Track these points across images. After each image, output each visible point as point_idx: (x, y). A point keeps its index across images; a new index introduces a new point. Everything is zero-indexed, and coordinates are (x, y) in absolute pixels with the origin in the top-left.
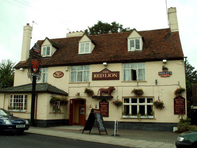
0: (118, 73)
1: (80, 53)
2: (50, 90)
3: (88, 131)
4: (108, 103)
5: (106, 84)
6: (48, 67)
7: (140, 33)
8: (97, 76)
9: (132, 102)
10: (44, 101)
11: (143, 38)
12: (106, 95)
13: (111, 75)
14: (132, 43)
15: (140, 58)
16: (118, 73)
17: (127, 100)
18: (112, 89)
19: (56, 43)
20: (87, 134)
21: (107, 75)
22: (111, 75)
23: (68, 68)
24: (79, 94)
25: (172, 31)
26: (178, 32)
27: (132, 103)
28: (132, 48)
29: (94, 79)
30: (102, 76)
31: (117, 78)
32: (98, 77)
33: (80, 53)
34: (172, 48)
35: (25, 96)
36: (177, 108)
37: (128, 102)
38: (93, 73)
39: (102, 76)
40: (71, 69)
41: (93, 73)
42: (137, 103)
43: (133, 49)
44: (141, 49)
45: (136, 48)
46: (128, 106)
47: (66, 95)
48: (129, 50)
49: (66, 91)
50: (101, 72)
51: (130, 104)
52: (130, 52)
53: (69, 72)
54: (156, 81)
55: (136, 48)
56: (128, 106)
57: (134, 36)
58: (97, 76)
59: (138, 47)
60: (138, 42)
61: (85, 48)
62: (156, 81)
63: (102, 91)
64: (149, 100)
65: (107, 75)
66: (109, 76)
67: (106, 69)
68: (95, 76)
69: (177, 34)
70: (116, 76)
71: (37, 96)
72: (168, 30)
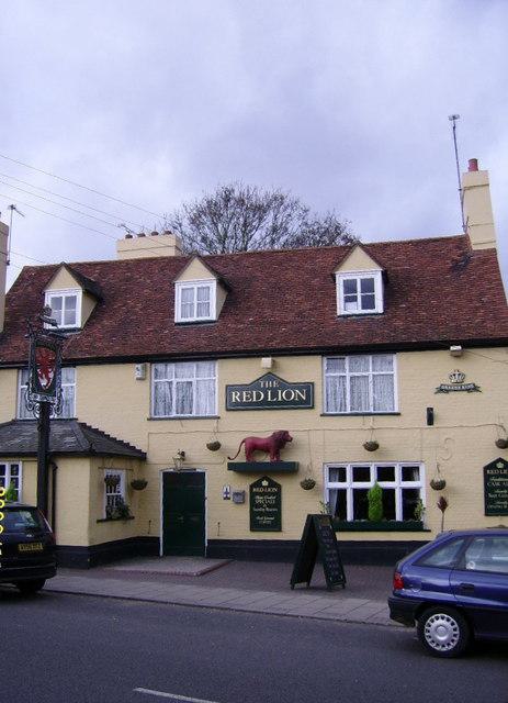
0: (308, 388)
1: (178, 318)
2: (100, 448)
3: (304, 585)
4: (279, 487)
5: (264, 424)
6: (215, 359)
7: (376, 251)
8: (241, 397)
9: (356, 479)
10: (76, 483)
11: (384, 274)
12: (266, 459)
13: (288, 395)
14: (350, 287)
15: (377, 341)
16: (308, 388)
17: (340, 474)
18: (282, 440)
19: (96, 280)
20: (302, 589)
21: (275, 395)
22: (288, 395)
23: (144, 369)
24: (183, 454)
25: (474, 248)
26: (494, 250)
27: (354, 481)
28: (350, 305)
29: (232, 407)
30: (258, 396)
31: (307, 403)
32: (247, 398)
33: (178, 318)
34: (477, 308)
35: (12, 466)
36: (261, 494)
37: (343, 479)
38: (229, 389)
39: (258, 396)
40: (325, 365)
41: (229, 389)
42: (394, 480)
43: (356, 309)
44: (379, 307)
45: (363, 308)
46: (342, 493)
47: (141, 457)
48: (341, 311)
49: (140, 445)
50: (255, 385)
51: (350, 485)
52: (344, 316)
53: (147, 383)
54: (430, 411)
55: (363, 308)
56: (342, 493)
57: (358, 268)
58: (241, 397)
59: (368, 302)
60: (368, 285)
61: (196, 302)
62: (430, 411)
63: (253, 447)
64: (409, 473)
65: (275, 395)
66: (282, 395)
67: (270, 376)
68: (235, 397)
69: (490, 258)
70: (304, 399)
71: (55, 469)
72: (461, 242)
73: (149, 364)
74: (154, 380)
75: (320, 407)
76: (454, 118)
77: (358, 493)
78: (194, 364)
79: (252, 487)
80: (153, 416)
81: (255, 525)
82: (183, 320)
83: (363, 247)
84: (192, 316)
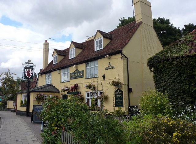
29: (72, 78)
50: (74, 73)
67: (77, 70)
75: (84, 78)
80: (86, 78)
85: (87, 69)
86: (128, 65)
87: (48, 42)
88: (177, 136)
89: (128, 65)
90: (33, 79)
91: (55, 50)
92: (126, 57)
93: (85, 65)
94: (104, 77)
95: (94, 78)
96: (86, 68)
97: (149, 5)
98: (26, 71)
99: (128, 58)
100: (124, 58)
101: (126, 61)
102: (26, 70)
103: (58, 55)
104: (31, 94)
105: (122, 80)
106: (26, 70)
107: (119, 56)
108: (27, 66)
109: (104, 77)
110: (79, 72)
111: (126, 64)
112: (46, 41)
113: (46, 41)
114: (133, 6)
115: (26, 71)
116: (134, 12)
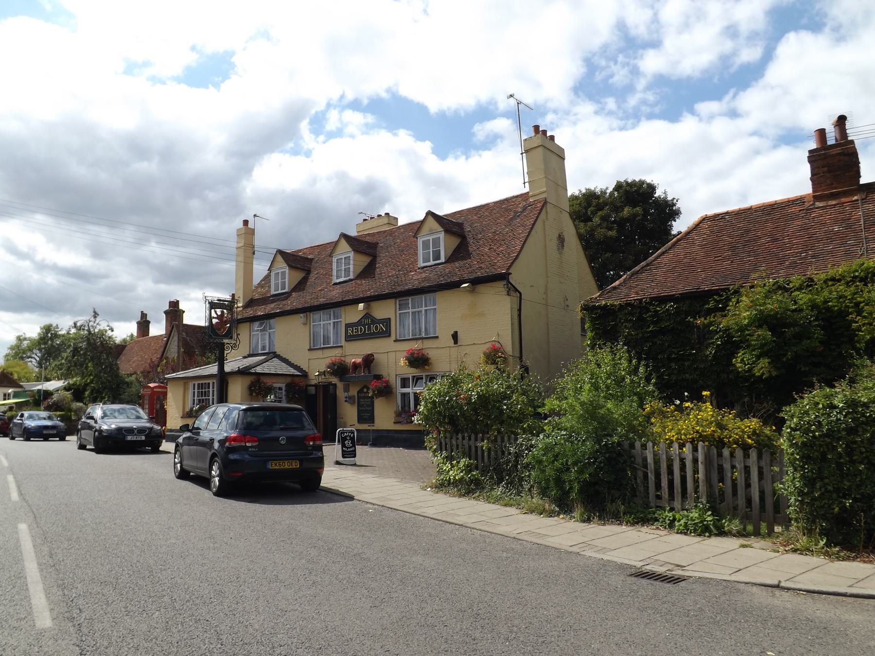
0: (387, 322)
8: (352, 332)
21: (369, 329)
29: (349, 338)
31: (387, 334)
50: (359, 323)
54: (456, 342)
62: (456, 342)
67: (368, 316)
73: (308, 313)
74: (312, 324)
75: (393, 337)
76: (266, 35)
77: (202, 389)
78: (343, 307)
79: (358, 393)
80: (398, 338)
81: (360, 420)
82: (338, 281)
83: (656, 15)
84: (278, 290)
85: (400, 313)
86: (520, 310)
87: (250, 225)
88: (644, 441)
89: (520, 310)
90: (231, 338)
91: (280, 252)
92: (516, 290)
93: (396, 304)
94: (455, 336)
95: (424, 340)
96: (398, 312)
97: (560, 155)
98: (215, 316)
99: (520, 293)
100: (512, 293)
101: (516, 300)
102: (213, 310)
103: (290, 266)
104: (230, 381)
105: (508, 345)
106: (213, 310)
107: (500, 286)
108: (218, 300)
109: (455, 336)
110: (375, 321)
111: (516, 307)
112: (246, 222)
113: (246, 222)
114: (524, 154)
115: (214, 315)
116: (526, 171)
